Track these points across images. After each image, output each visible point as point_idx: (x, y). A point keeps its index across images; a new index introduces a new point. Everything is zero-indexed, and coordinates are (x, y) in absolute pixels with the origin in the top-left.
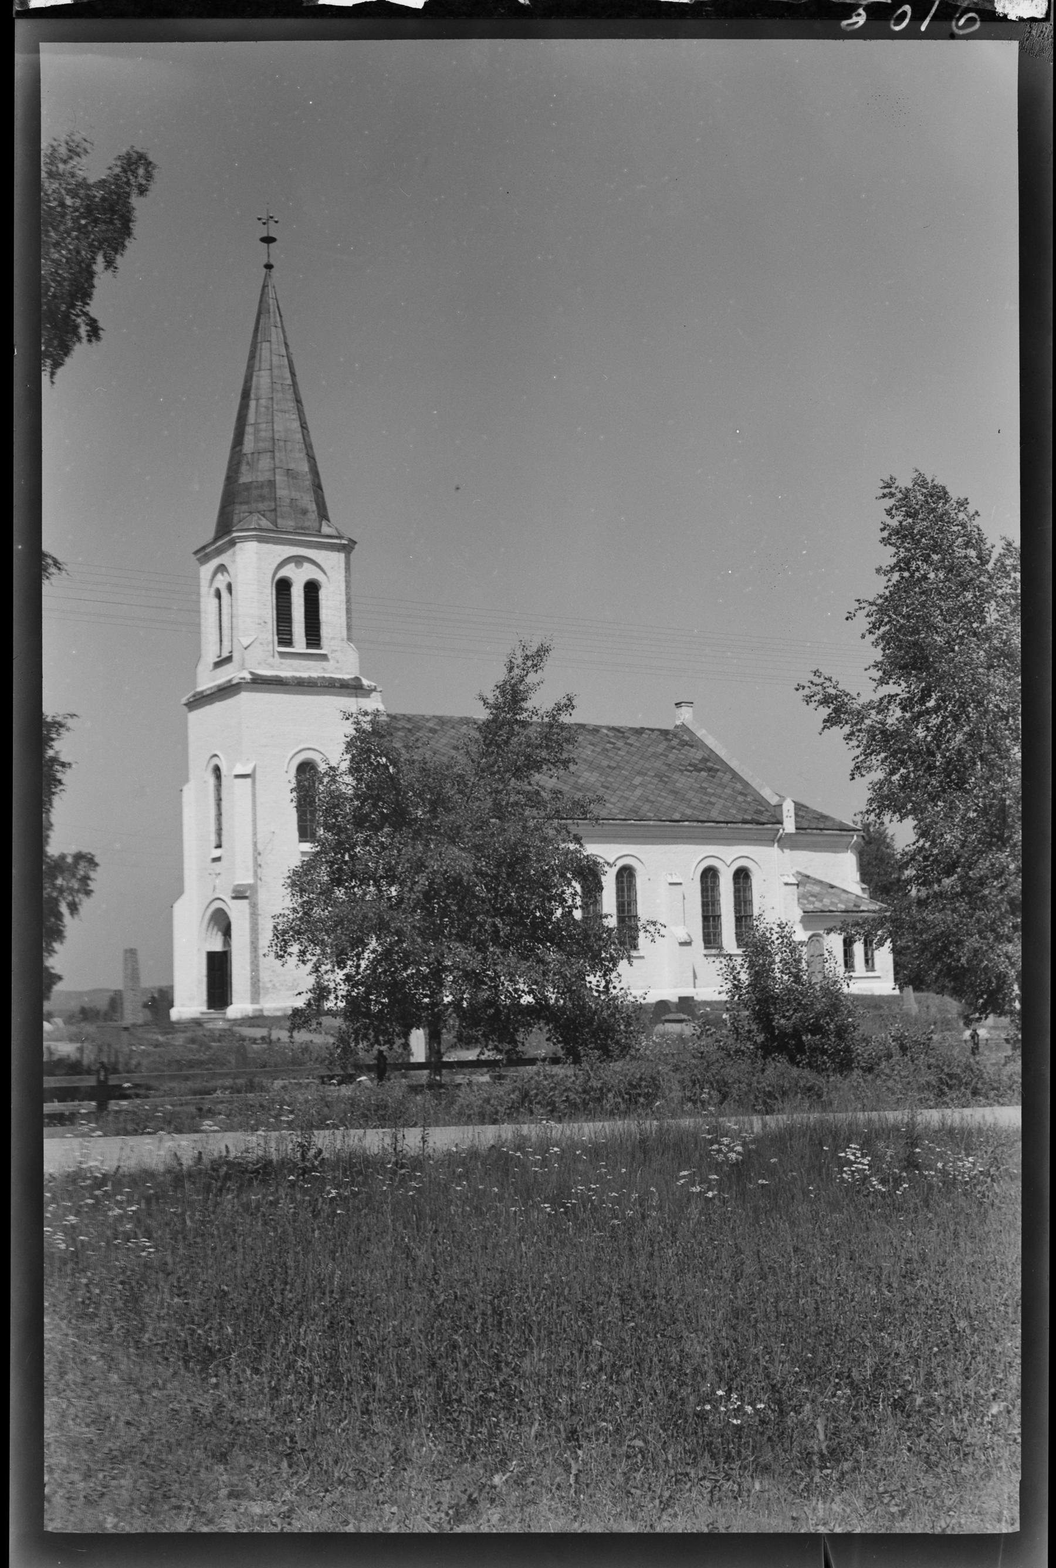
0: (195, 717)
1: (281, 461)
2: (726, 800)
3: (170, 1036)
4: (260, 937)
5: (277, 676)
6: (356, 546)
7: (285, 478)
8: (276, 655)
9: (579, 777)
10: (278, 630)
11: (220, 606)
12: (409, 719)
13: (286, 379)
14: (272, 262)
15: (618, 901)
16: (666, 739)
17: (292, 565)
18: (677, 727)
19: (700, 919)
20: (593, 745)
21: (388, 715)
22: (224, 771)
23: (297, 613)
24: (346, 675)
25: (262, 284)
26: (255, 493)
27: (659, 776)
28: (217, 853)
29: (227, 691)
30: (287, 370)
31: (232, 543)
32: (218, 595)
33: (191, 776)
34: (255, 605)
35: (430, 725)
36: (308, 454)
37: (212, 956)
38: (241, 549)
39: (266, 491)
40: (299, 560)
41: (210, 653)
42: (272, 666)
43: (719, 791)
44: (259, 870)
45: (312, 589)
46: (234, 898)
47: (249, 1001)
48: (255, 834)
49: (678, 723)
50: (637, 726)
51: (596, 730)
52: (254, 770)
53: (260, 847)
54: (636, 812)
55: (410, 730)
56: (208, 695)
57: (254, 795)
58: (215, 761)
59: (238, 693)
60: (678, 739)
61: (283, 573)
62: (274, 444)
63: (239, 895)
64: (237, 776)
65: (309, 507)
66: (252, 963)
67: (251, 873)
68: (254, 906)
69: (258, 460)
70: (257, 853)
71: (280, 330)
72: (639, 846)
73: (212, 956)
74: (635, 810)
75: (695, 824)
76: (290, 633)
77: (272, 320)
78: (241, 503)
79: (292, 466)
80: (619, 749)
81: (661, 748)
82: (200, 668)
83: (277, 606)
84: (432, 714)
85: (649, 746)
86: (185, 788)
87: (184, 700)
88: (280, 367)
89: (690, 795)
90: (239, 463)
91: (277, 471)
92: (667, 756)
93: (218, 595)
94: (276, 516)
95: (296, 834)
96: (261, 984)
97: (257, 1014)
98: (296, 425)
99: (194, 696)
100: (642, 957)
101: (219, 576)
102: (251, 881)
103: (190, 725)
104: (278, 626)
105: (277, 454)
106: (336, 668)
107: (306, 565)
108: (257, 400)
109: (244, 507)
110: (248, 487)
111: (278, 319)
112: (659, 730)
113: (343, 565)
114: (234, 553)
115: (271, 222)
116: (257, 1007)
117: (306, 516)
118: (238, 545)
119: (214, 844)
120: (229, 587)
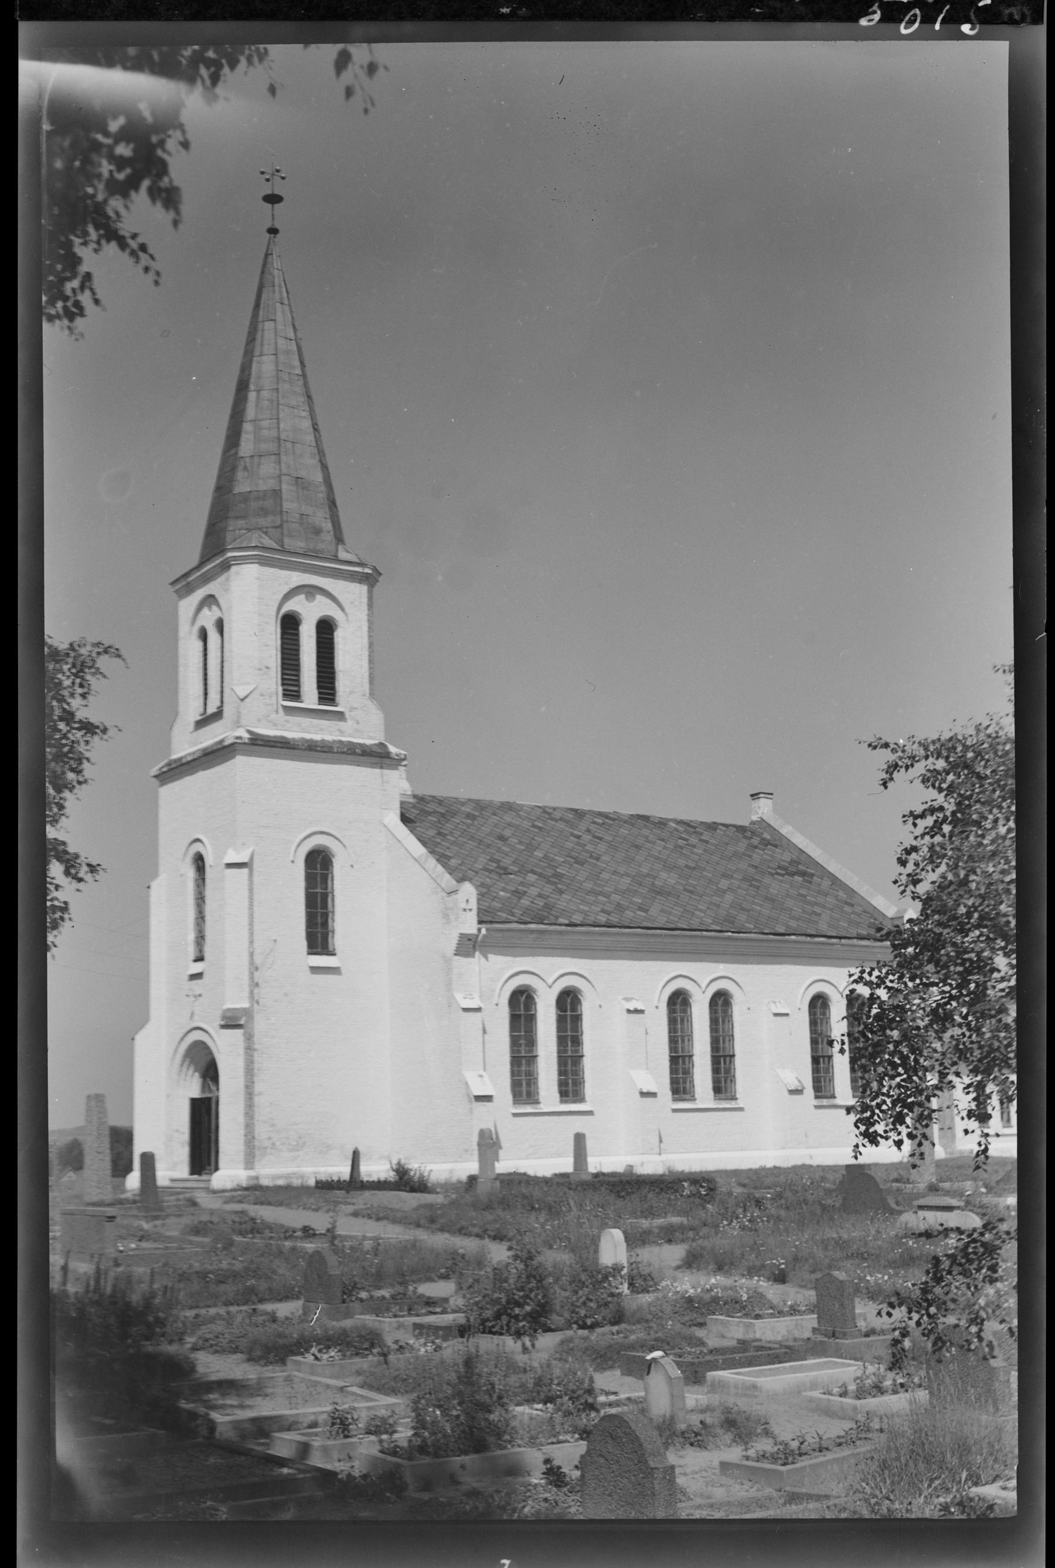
0: (168, 792)
1: (288, 467)
2: (831, 910)
3: (159, 1222)
4: (256, 1079)
5: (282, 737)
6: (381, 579)
7: (294, 488)
8: (281, 710)
9: (655, 878)
10: (283, 679)
11: (205, 649)
12: (440, 802)
13: (294, 367)
14: (277, 226)
15: (712, 1036)
16: (746, 837)
17: (303, 596)
18: (753, 823)
19: (809, 1060)
20: (663, 840)
21: (415, 796)
22: (209, 860)
23: (306, 658)
24: (369, 739)
25: (264, 252)
26: (254, 505)
27: (748, 879)
28: (197, 968)
29: (216, 755)
30: (296, 357)
31: (226, 566)
32: (203, 635)
33: (161, 869)
34: (253, 648)
35: (467, 809)
36: (320, 461)
37: (194, 1102)
38: (237, 573)
39: (269, 503)
40: (310, 591)
41: (191, 708)
42: (275, 725)
43: (820, 899)
44: (256, 991)
45: (326, 629)
46: (223, 1027)
47: (242, 1166)
48: (251, 942)
49: (755, 818)
50: (709, 819)
51: (662, 823)
52: (252, 858)
53: (258, 960)
54: (732, 923)
55: (443, 815)
56: (189, 762)
57: (251, 890)
58: (197, 847)
59: (233, 757)
60: (759, 837)
61: (290, 606)
62: (279, 446)
63: (231, 1022)
64: (229, 866)
65: (323, 525)
66: (246, 1114)
67: (246, 994)
68: (249, 1038)
69: (259, 464)
70: (254, 968)
71: (287, 308)
72: (736, 966)
73: (194, 1102)
74: (730, 920)
75: (803, 938)
76: (297, 683)
77: (277, 296)
78: (237, 518)
79: (302, 473)
80: (694, 846)
81: (742, 846)
82: (176, 730)
83: (283, 648)
84: (467, 797)
85: (727, 844)
86: (154, 885)
87: (155, 771)
88: (287, 352)
89: (789, 903)
90: (234, 469)
91: (283, 478)
92: (750, 857)
93: (203, 635)
94: (282, 534)
95: (304, 944)
96: (256, 1143)
97: (252, 1183)
98: (307, 424)
99: (169, 764)
100: (741, 1109)
101: (205, 611)
102: (245, 1005)
103: (161, 803)
104: (283, 674)
105: (283, 458)
106: (357, 731)
107: (319, 598)
108: (258, 391)
109: (241, 523)
110: (246, 497)
111: (285, 295)
112: (734, 826)
113: (365, 600)
114: (227, 580)
115: (277, 179)
116: (252, 1173)
117: (313, 541)
118: (234, 569)
119: (192, 957)
120: (220, 625)
